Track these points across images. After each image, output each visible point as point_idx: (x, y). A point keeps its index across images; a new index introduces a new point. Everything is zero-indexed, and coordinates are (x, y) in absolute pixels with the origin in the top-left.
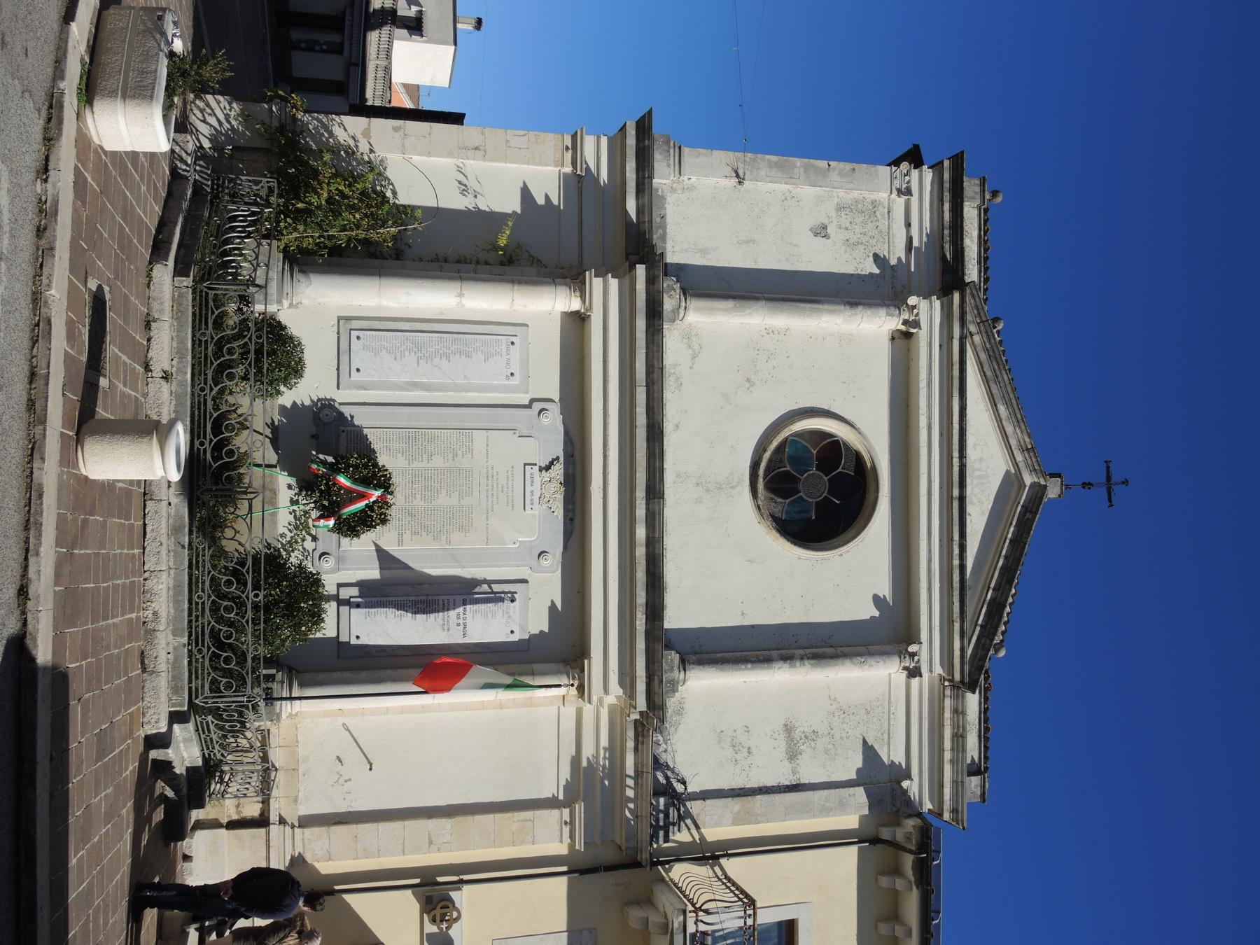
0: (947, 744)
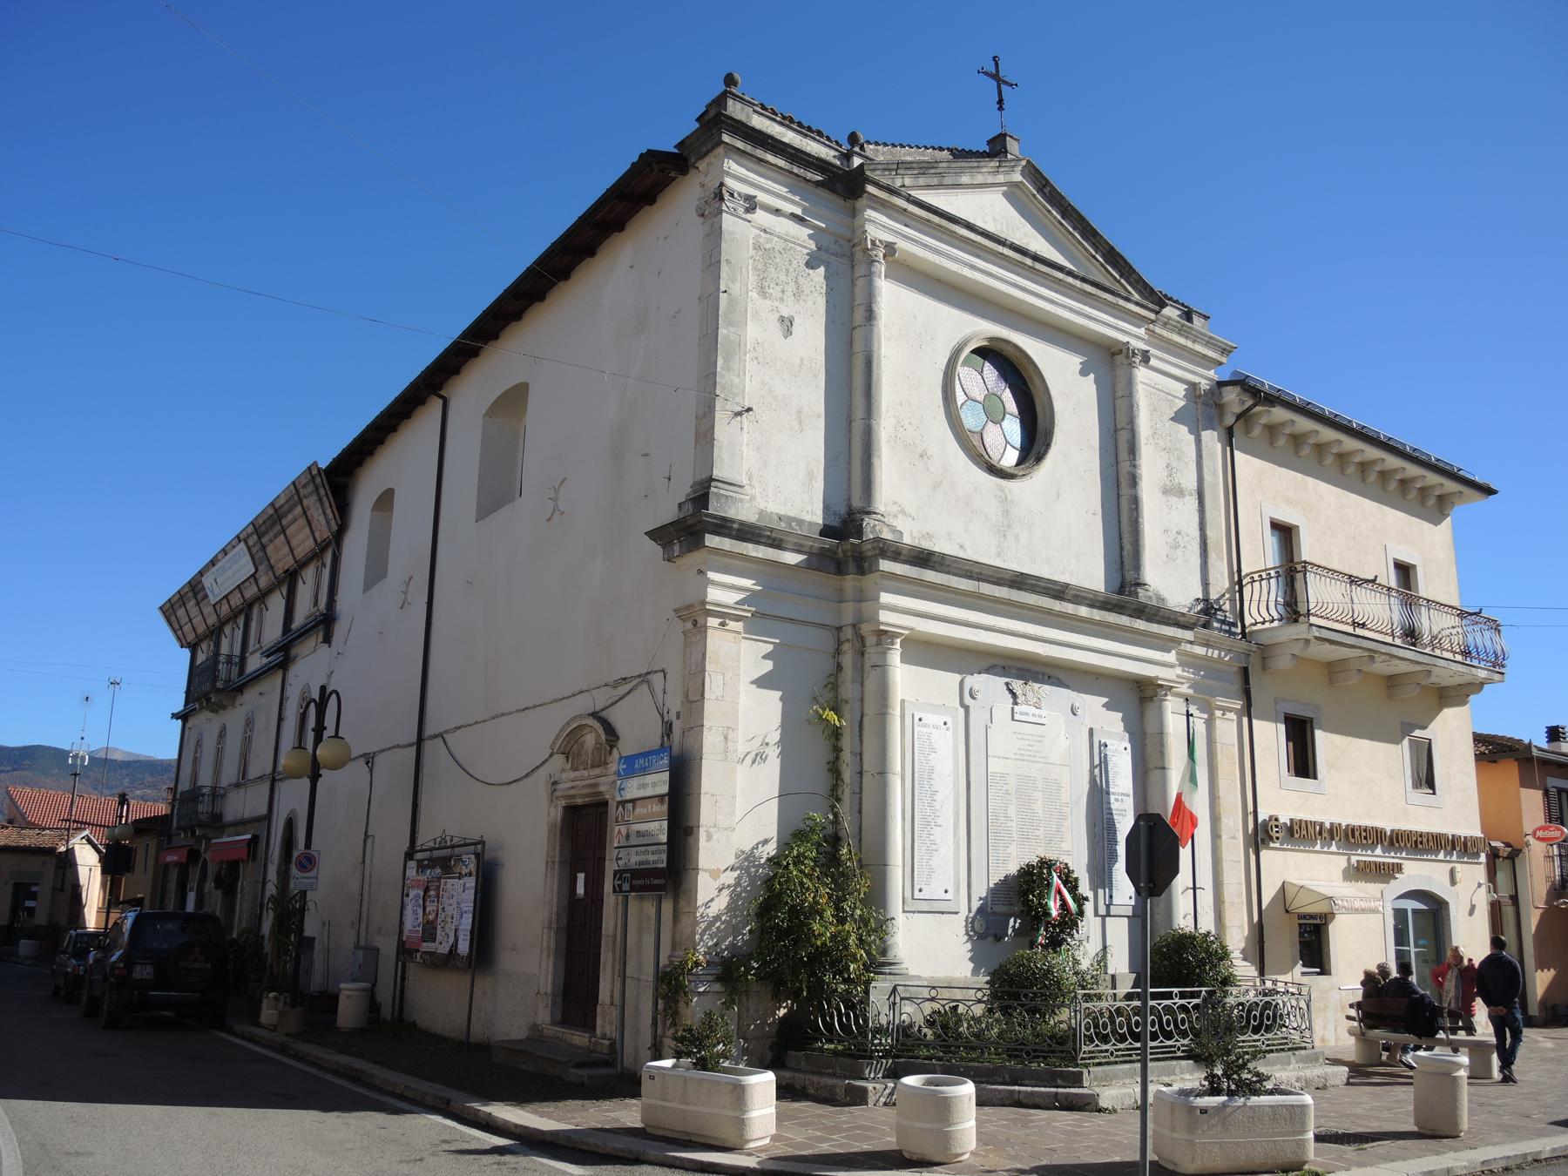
0: (1182, 341)
